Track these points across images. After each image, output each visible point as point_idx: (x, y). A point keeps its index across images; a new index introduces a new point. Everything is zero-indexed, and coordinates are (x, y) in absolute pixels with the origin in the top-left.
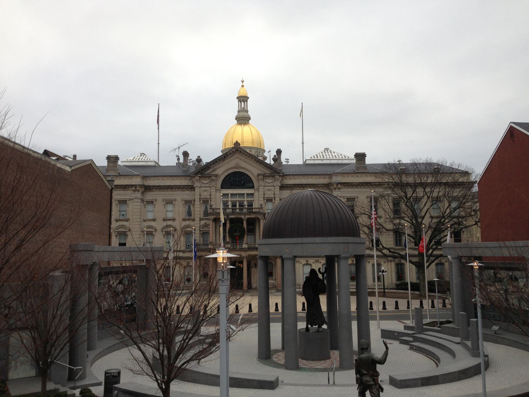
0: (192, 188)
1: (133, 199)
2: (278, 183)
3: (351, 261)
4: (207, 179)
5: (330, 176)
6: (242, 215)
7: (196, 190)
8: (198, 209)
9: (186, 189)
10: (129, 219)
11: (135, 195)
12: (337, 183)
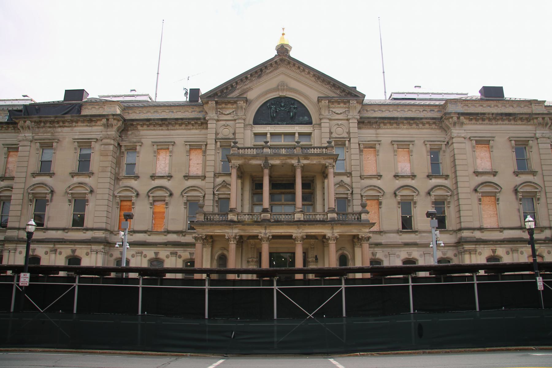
0: (202, 123)
1: (102, 140)
2: (354, 114)
4: (229, 106)
6: (292, 159)
7: (209, 126)
8: (212, 158)
9: (193, 125)
12: (459, 114)
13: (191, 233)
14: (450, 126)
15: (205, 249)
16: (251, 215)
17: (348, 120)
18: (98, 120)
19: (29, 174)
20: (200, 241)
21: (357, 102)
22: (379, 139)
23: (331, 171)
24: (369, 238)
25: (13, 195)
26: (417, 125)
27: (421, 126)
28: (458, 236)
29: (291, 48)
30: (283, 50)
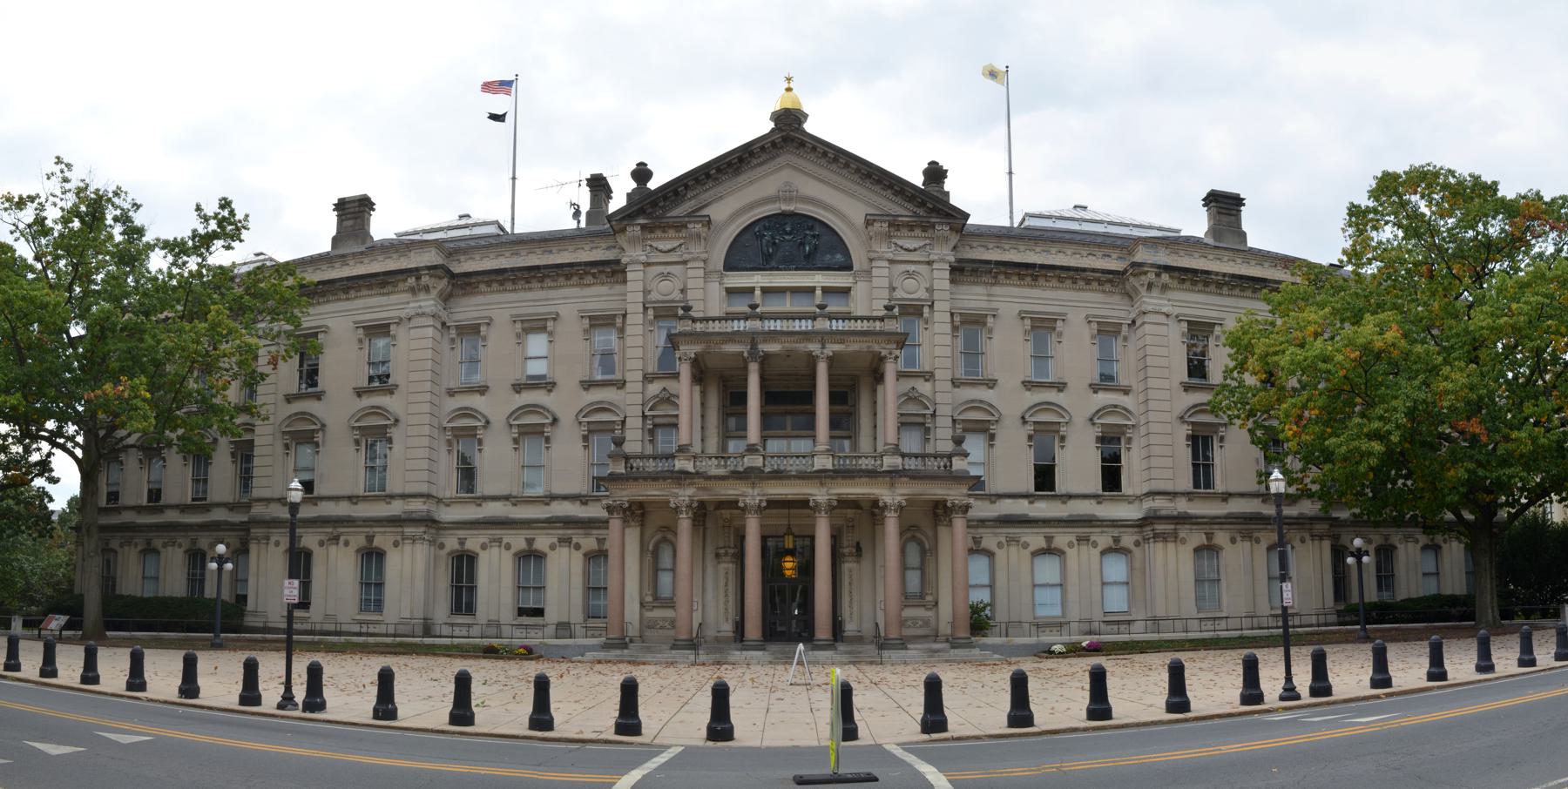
0: (613, 271)
1: (410, 319)
2: (944, 254)
3: (1204, 536)
4: (672, 233)
5: (1125, 252)
7: (630, 276)
9: (594, 276)
10: (397, 386)
11: (417, 304)
12: (1159, 267)
13: (598, 499)
14: (1140, 288)
15: (628, 531)
16: (722, 457)
17: (929, 263)
18: (398, 281)
19: (280, 397)
20: (618, 514)
21: (951, 229)
22: (994, 305)
23: (890, 370)
24: (967, 508)
25: (256, 438)
26: (1075, 282)
27: (1081, 283)
28: (1144, 507)
29: (806, 116)
30: (789, 122)
